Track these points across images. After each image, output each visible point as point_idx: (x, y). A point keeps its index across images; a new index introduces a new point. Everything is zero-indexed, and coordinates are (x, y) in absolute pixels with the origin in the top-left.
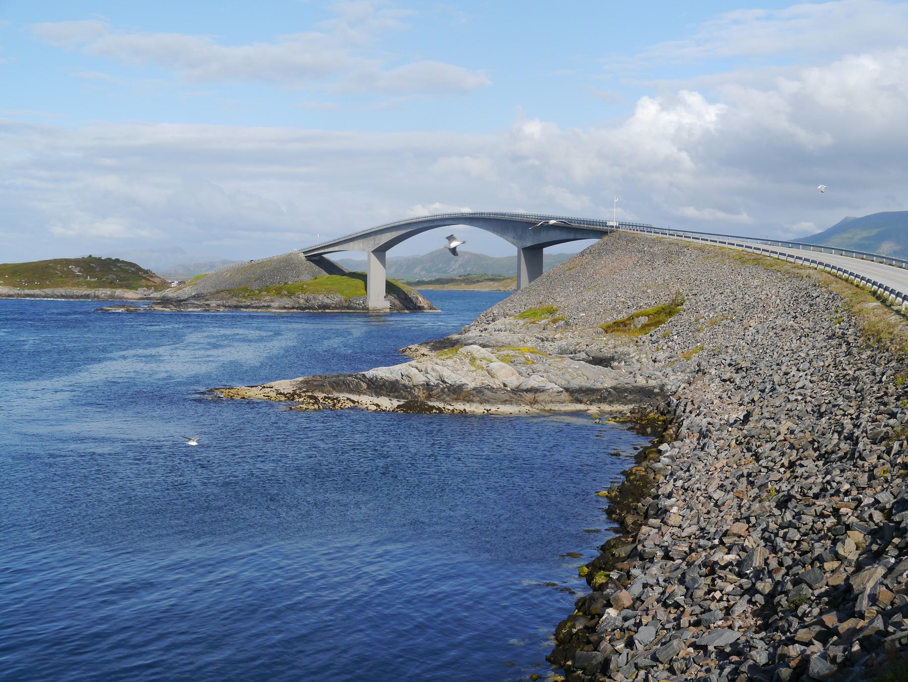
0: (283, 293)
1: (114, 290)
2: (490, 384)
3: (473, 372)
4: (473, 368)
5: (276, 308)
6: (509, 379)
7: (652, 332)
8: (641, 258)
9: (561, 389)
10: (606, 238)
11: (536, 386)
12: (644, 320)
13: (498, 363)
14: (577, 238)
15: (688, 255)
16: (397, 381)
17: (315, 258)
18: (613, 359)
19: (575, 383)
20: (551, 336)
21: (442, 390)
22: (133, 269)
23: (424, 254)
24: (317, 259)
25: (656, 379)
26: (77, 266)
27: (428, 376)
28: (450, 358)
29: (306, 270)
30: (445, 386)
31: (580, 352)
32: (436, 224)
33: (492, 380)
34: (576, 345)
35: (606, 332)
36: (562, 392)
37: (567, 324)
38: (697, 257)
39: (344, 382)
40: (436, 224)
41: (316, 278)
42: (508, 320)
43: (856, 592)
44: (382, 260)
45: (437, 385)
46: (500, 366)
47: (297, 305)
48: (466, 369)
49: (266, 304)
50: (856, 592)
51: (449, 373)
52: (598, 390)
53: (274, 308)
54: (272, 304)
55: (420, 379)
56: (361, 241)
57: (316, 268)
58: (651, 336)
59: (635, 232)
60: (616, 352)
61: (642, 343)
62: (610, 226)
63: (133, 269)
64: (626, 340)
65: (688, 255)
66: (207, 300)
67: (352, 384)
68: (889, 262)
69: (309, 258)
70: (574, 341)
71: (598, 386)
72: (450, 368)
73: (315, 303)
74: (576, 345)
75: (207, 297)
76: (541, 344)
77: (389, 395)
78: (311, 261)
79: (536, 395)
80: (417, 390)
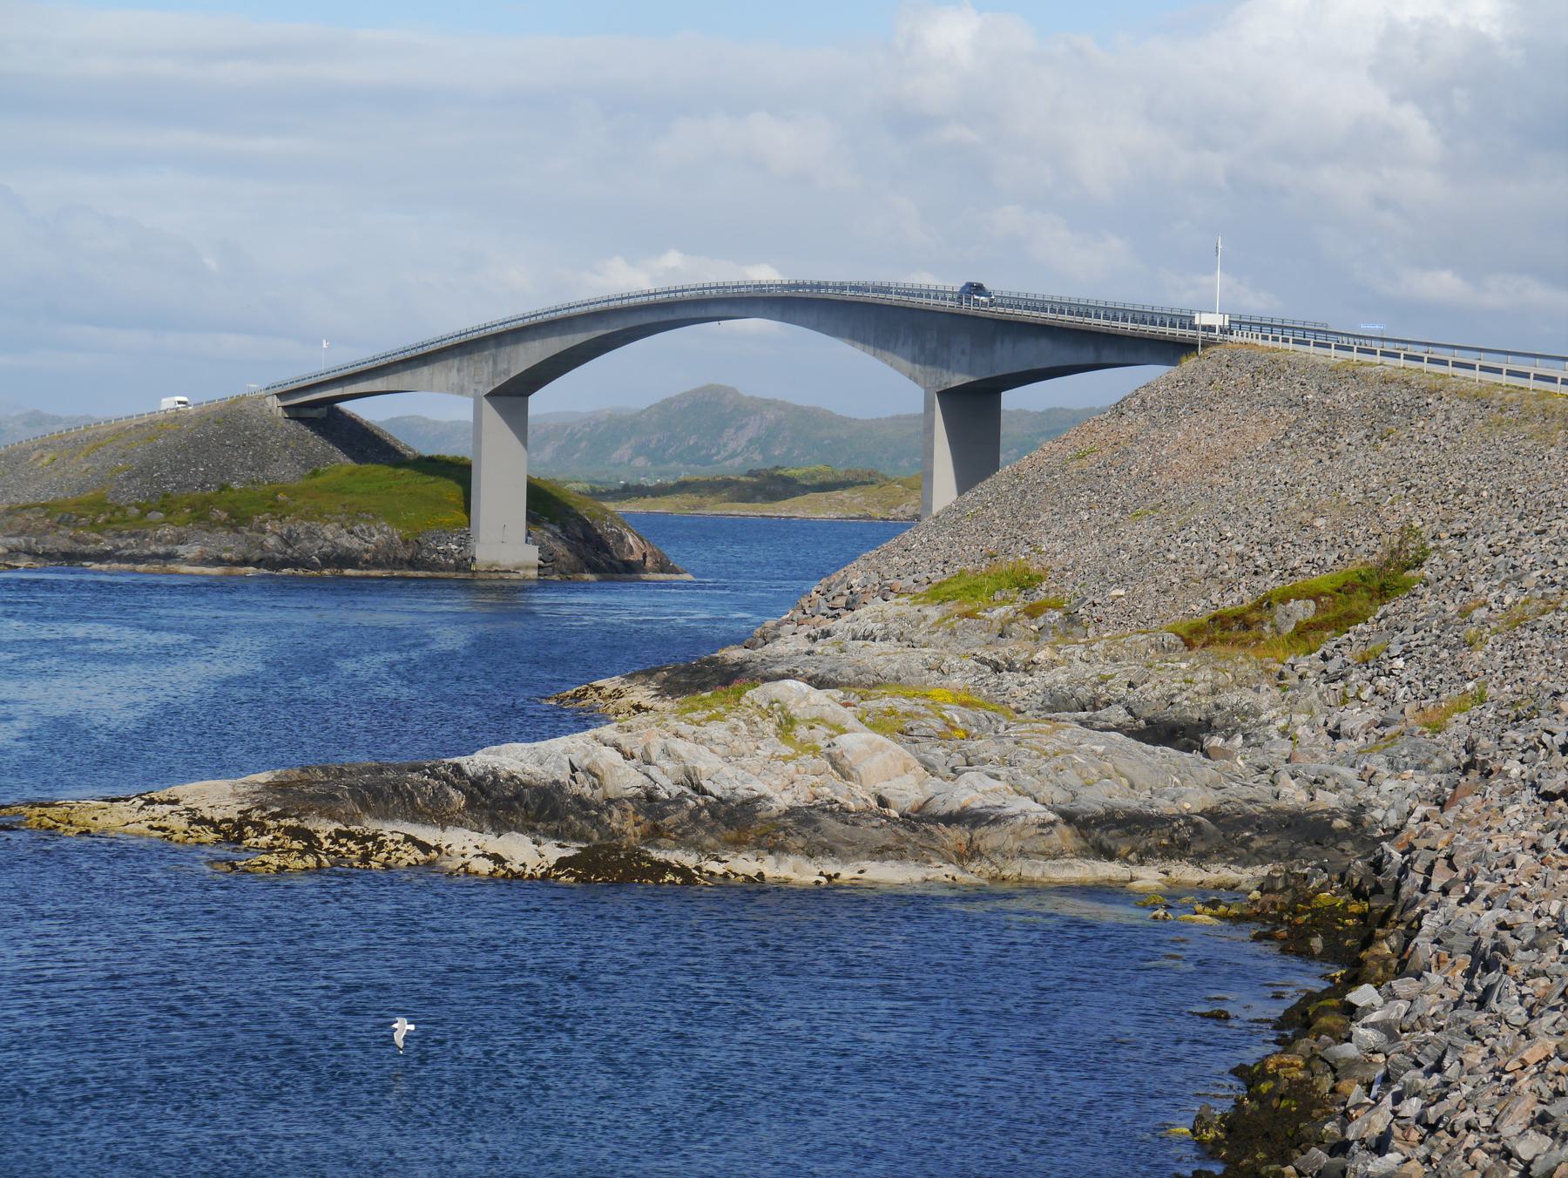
2: (839, 799)
3: (786, 760)
4: (786, 750)
5: (193, 562)
6: (896, 783)
7: (1328, 648)
9: (1052, 816)
11: (977, 805)
12: (1303, 610)
14: (1104, 361)
15: (1440, 416)
17: (314, 413)
21: (694, 815)
23: (644, 406)
27: (652, 771)
28: (719, 717)
29: (286, 447)
31: (1108, 704)
32: (680, 314)
34: (1096, 685)
35: (1189, 645)
36: (1053, 824)
37: (1071, 619)
40: (680, 314)
41: (315, 474)
44: (517, 419)
46: (870, 743)
47: (256, 554)
48: (765, 752)
49: (161, 550)
52: (1162, 820)
54: (181, 549)
55: (626, 779)
56: (455, 362)
60: (1218, 707)
61: (1296, 681)
62: (1204, 328)
64: (1248, 669)
65: (1440, 416)
67: (422, 795)
71: (1164, 806)
72: (717, 749)
74: (1096, 685)
79: (977, 832)
80: (616, 813)
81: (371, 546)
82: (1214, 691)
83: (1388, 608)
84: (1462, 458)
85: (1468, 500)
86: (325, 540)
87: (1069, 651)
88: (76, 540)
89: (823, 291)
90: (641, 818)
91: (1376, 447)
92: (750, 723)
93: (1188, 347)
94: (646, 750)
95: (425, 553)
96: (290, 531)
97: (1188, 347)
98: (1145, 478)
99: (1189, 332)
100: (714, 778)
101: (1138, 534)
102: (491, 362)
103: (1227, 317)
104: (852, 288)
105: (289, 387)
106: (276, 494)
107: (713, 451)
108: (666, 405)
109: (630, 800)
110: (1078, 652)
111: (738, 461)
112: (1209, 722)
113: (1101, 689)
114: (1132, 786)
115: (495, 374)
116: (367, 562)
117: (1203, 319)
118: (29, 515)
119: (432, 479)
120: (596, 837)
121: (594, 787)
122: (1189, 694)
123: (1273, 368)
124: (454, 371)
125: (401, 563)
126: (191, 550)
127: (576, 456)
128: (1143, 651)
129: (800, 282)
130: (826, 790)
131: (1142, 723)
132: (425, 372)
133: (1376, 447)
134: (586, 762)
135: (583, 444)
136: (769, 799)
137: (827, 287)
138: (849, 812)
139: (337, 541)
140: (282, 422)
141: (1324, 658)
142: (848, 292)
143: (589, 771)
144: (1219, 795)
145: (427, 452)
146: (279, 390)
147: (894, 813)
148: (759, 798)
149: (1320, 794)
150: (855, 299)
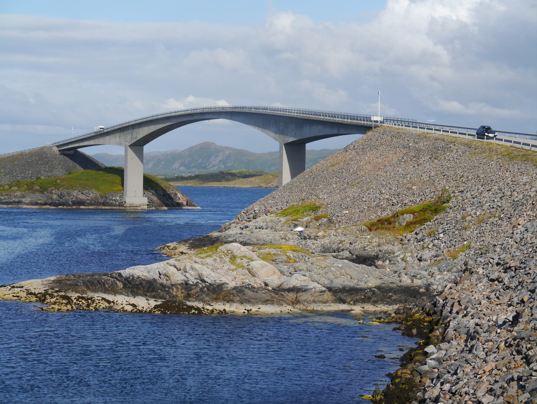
2: (251, 283)
3: (233, 270)
4: (233, 267)
5: (27, 204)
6: (271, 278)
7: (417, 230)
9: (324, 289)
10: (370, 133)
11: (298, 285)
12: (409, 218)
14: (341, 133)
15: (455, 151)
17: (69, 152)
19: (339, 282)
20: (314, 234)
21: (202, 290)
27: (187, 274)
28: (210, 256)
29: (60, 164)
31: (343, 250)
32: (195, 118)
33: (252, 279)
34: (339, 244)
36: (324, 291)
37: (330, 221)
40: (195, 118)
41: (70, 173)
42: (269, 218)
44: (140, 154)
45: (196, 285)
46: (261, 264)
48: (226, 268)
49: (17, 200)
52: (362, 290)
54: (23, 200)
55: (178, 277)
57: (70, 163)
60: (380, 251)
61: (407, 242)
62: (375, 121)
64: (390, 238)
65: (455, 151)
67: (108, 284)
69: (63, 152)
71: (362, 285)
72: (209, 267)
74: (339, 244)
78: (65, 155)
79: (299, 295)
80: (175, 289)
81: (90, 198)
82: (379, 246)
86: (74, 196)
87: (329, 232)
89: (244, 109)
90: (183, 291)
91: (433, 162)
93: (369, 128)
94: (185, 267)
95: (108, 200)
96: (61, 193)
97: (369, 128)
99: (369, 123)
100: (208, 277)
101: (352, 192)
102: (130, 134)
103: (382, 118)
104: (254, 108)
105: (61, 143)
106: (57, 180)
107: (207, 165)
108: (191, 149)
110: (333, 232)
111: (216, 168)
112: (377, 256)
113: (340, 245)
114: (351, 278)
115: (132, 138)
116: (88, 203)
117: (374, 118)
119: (111, 175)
120: (168, 297)
121: (167, 280)
123: (398, 135)
124: (118, 138)
125: (100, 204)
126: (27, 200)
127: (160, 166)
128: (355, 232)
129: (237, 106)
130: (247, 281)
131: (355, 256)
132: (108, 138)
133: (433, 162)
134: (164, 272)
135: (162, 163)
136: (227, 284)
137: (246, 108)
138: (255, 288)
139: (78, 196)
140: (58, 156)
142: (253, 110)
143: (165, 275)
144: (381, 281)
145: (108, 165)
146: (57, 144)
147: (270, 288)
148: (224, 283)
149: (415, 280)
150: (255, 112)
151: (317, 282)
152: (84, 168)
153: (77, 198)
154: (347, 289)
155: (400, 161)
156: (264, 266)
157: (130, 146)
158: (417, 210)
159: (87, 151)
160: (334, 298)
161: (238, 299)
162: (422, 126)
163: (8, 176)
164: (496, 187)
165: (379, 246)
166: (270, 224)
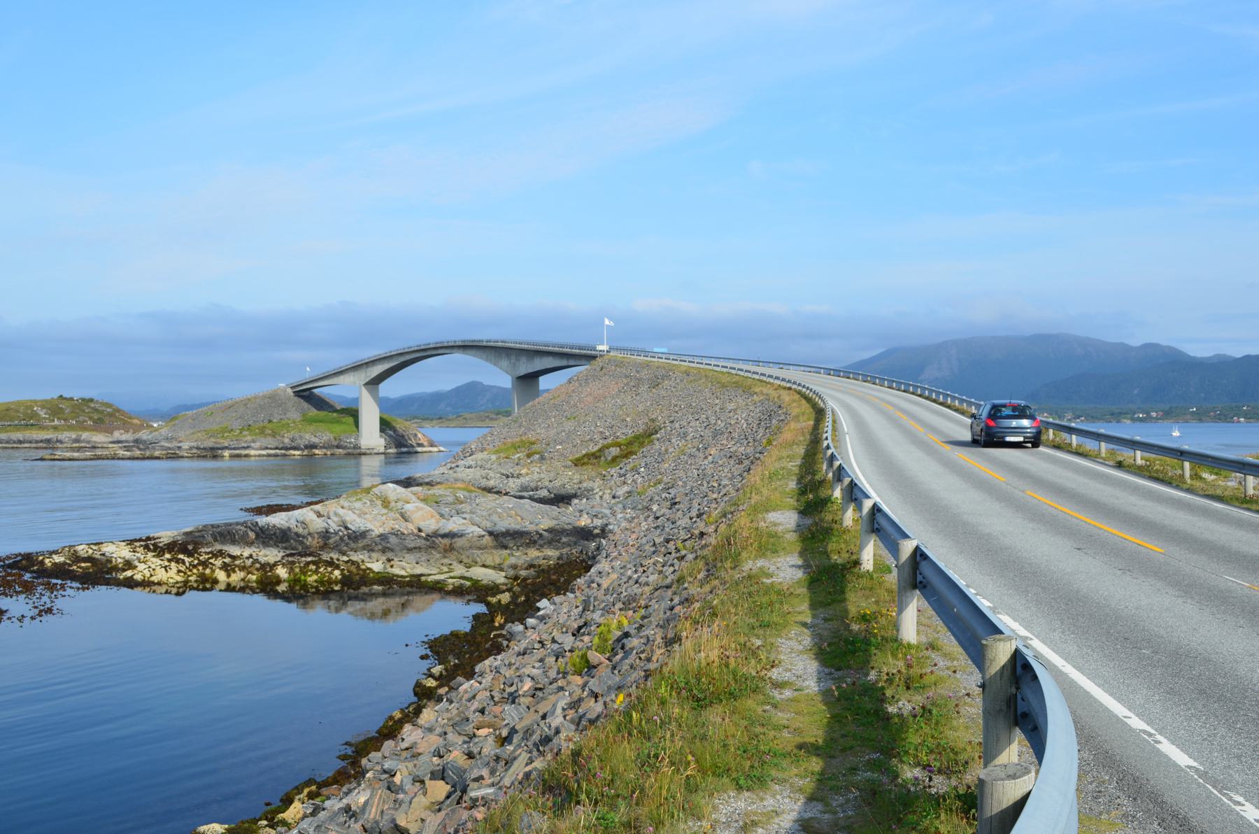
0: (266, 433)
1: (80, 433)
2: (401, 530)
3: (382, 515)
4: (385, 511)
5: (257, 449)
6: (427, 522)
7: (621, 465)
8: (627, 384)
9: (484, 533)
11: (455, 530)
12: (614, 451)
13: (417, 504)
14: (570, 364)
15: (673, 379)
16: (289, 529)
17: (305, 394)
18: (575, 496)
19: (503, 525)
20: (517, 472)
21: (341, 539)
22: (108, 410)
24: (306, 394)
25: (602, 517)
26: (43, 407)
27: (329, 521)
28: (360, 499)
30: (345, 533)
31: (541, 488)
33: (404, 524)
34: (537, 482)
35: (576, 465)
36: (483, 536)
37: (542, 458)
38: (681, 381)
39: (229, 532)
42: (484, 455)
43: (816, 764)
45: (336, 533)
46: (417, 507)
47: (281, 445)
48: (376, 512)
49: (245, 445)
50: (816, 764)
51: (354, 517)
52: (528, 533)
53: (254, 449)
54: (253, 445)
55: (318, 524)
57: (305, 405)
58: (621, 468)
59: (625, 356)
60: (579, 488)
61: (609, 478)
62: (600, 351)
63: (108, 410)
64: (593, 474)
65: (673, 379)
66: (180, 442)
67: (238, 534)
68: (837, 373)
69: (299, 394)
70: (536, 476)
71: (532, 528)
72: (357, 512)
73: (302, 443)
74: (537, 482)
75: (181, 439)
76: (505, 482)
77: (278, 546)
78: (299, 396)
79: (453, 541)
80: (310, 539)
82: (580, 483)
83: (645, 449)
84: (677, 394)
85: (677, 409)
88: (216, 443)
90: (320, 540)
91: (651, 391)
92: (371, 501)
93: (594, 357)
94: (328, 513)
97: (594, 357)
98: (575, 405)
99: (593, 352)
101: (569, 426)
104: (502, 342)
109: (317, 533)
112: (576, 494)
113: (539, 483)
114: (522, 519)
117: (600, 348)
118: (199, 435)
120: (300, 548)
121: (304, 529)
122: (571, 484)
123: (620, 364)
126: (257, 445)
130: (397, 526)
131: (552, 495)
133: (651, 391)
134: (302, 519)
136: (373, 531)
138: (404, 534)
141: (621, 468)
143: (303, 523)
144: (556, 522)
147: (423, 534)
148: (368, 531)
149: (595, 520)
151: (477, 525)
152: (319, 410)
153: (309, 442)
154: (511, 532)
155: (620, 391)
156: (418, 509)
157: (366, 384)
158: (623, 442)
159: (321, 392)
160: (495, 543)
161: (380, 547)
162: (660, 355)
163: (239, 420)
164: (704, 416)
165: (580, 483)
166: (479, 463)
